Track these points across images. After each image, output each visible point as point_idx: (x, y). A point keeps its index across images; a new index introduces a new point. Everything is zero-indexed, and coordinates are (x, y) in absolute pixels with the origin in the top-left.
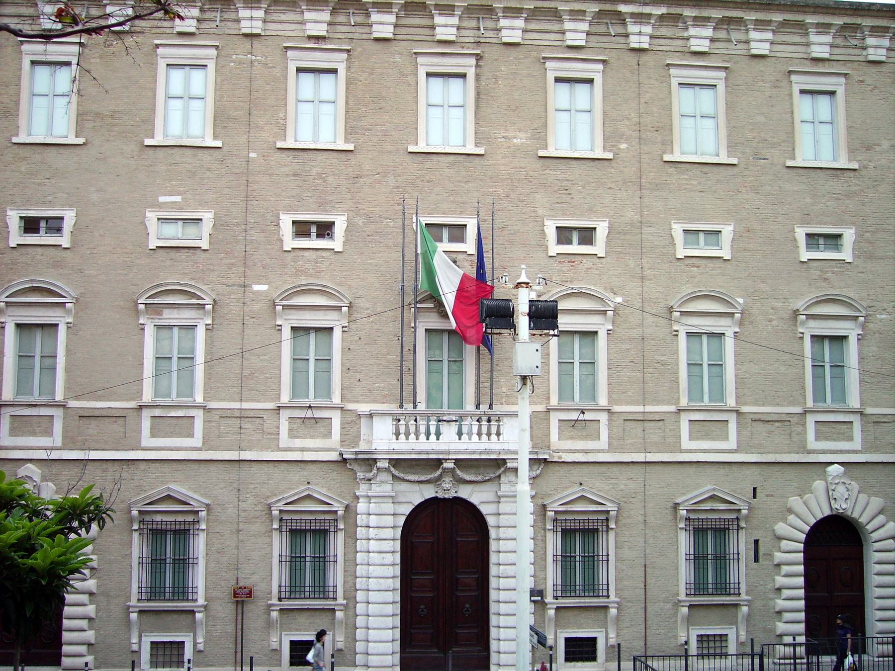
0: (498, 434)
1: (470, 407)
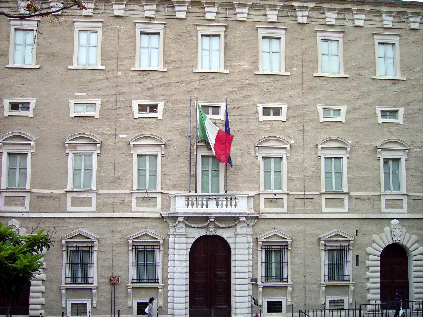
0: (236, 205)
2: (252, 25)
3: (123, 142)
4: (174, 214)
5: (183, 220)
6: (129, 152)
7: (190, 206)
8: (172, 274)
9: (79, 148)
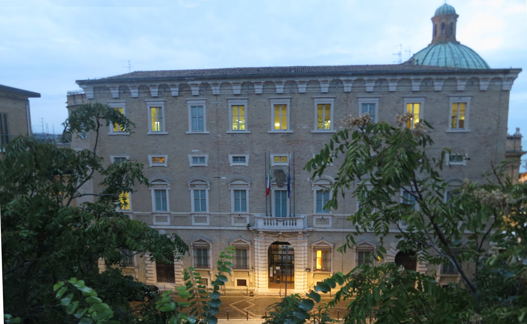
0: (296, 224)
1: (274, 216)
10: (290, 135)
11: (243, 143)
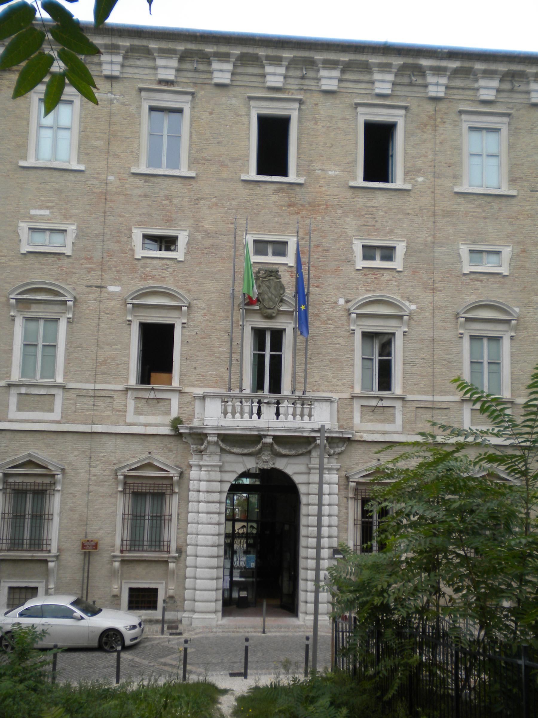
0: (310, 416)
2: (347, 100)
3: (115, 299)
4: (201, 428)
5: (215, 439)
6: (124, 318)
7: (229, 415)
8: (194, 536)
9: (34, 308)
10: (298, 189)
11: (175, 201)
